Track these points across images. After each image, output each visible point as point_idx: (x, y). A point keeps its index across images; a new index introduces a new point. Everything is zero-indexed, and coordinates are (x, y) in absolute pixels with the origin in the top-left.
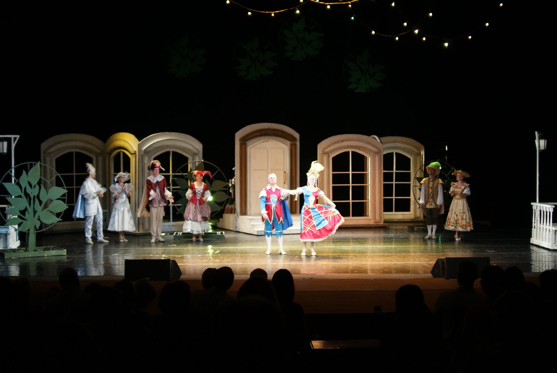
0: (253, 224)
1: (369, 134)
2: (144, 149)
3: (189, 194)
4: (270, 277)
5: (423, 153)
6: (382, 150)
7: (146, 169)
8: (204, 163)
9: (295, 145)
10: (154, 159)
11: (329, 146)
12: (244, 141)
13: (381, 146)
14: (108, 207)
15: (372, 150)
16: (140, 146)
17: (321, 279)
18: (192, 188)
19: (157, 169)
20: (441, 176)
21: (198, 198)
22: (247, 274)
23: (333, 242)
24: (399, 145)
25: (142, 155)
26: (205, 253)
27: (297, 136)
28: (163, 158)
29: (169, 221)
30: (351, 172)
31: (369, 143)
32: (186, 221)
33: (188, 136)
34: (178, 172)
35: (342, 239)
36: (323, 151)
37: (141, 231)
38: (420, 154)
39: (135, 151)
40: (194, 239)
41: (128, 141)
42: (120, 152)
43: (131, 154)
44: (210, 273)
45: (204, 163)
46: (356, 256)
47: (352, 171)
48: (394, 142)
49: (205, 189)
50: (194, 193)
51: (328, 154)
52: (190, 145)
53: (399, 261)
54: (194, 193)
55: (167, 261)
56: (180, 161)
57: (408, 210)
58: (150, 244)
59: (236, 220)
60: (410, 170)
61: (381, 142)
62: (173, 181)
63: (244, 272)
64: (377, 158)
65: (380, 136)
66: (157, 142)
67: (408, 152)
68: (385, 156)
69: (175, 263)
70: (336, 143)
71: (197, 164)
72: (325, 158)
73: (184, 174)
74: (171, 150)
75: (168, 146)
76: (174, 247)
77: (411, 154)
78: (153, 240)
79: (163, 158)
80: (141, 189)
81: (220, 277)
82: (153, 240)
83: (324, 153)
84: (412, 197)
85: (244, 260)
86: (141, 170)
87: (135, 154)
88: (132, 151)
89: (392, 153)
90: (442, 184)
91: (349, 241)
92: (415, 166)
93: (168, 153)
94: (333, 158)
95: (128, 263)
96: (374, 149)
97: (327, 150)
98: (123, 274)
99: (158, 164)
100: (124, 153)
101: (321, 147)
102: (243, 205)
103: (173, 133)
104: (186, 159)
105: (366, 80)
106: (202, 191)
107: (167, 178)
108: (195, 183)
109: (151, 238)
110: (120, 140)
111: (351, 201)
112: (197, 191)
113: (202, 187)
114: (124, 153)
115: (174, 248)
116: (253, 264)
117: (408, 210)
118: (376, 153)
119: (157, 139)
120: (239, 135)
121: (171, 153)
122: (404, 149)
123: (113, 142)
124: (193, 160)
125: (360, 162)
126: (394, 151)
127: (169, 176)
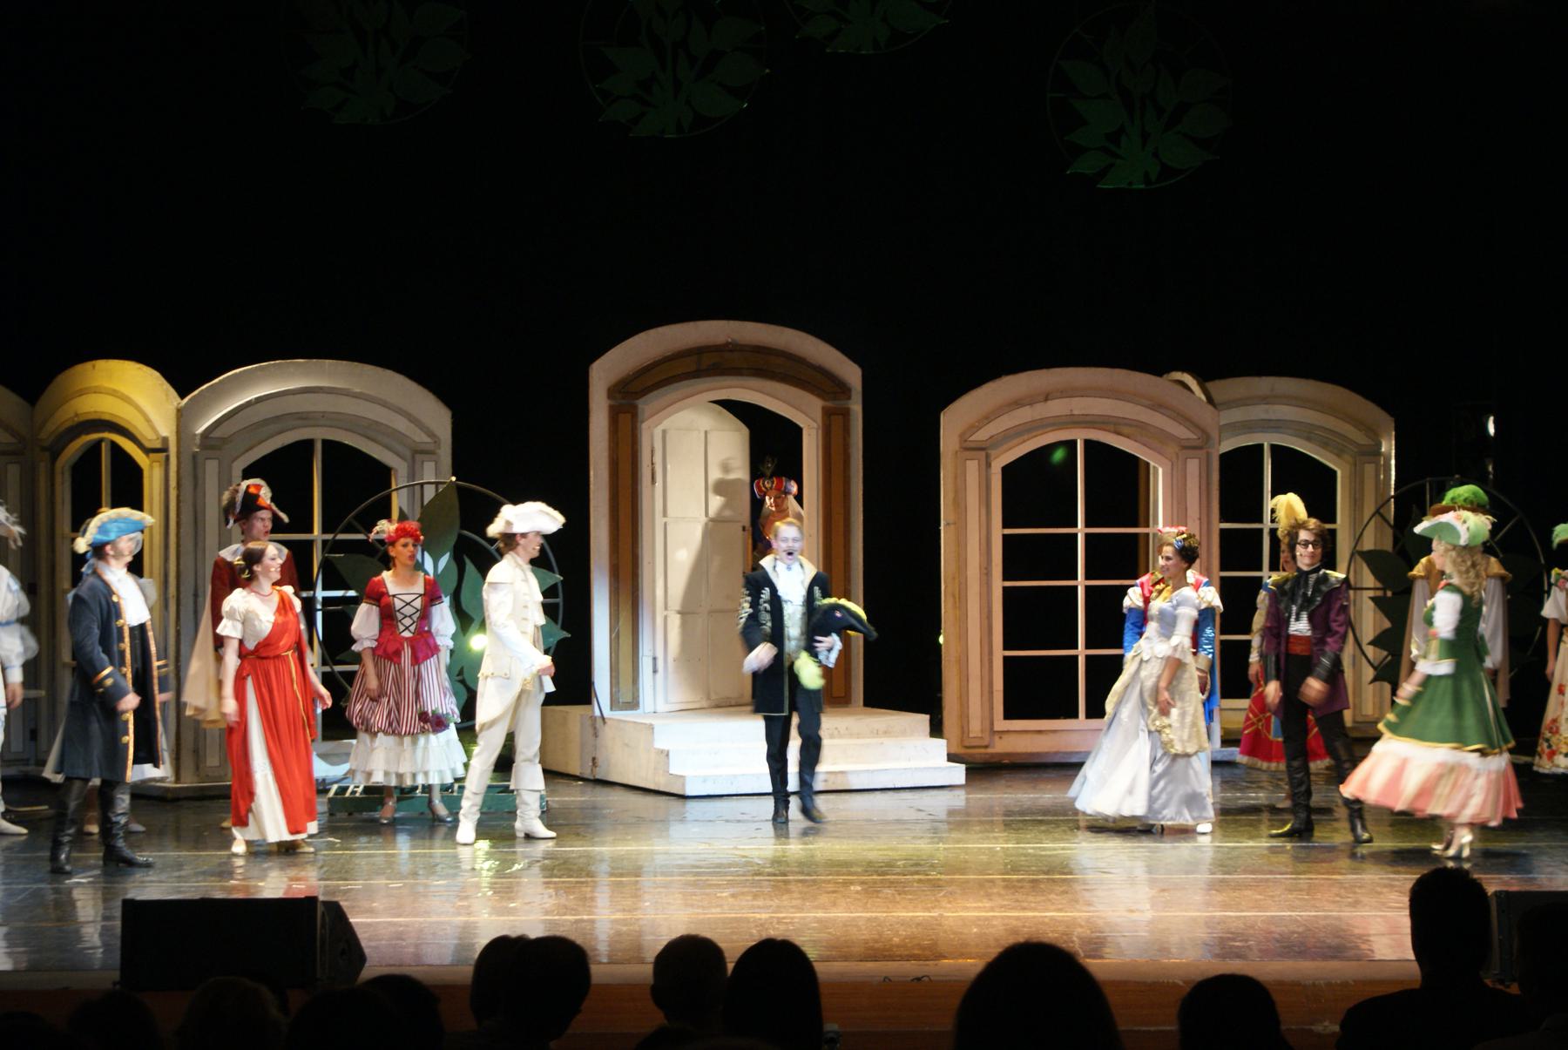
1: (1159, 371)
2: (200, 430)
4: (368, 972)
5: (1388, 446)
6: (1215, 434)
7: (212, 514)
8: (460, 489)
9: (846, 414)
10: (247, 474)
11: (988, 419)
12: (630, 395)
13: (1207, 415)
14: (44, 680)
15: (1167, 429)
17: (1137, 983)
19: (265, 514)
21: (407, 634)
22: (642, 961)
23: (1007, 825)
24: (1279, 412)
25: (194, 456)
27: (852, 373)
28: (284, 469)
30: (1081, 530)
31: (1158, 406)
32: (363, 736)
33: (389, 373)
35: (1046, 812)
36: (963, 438)
37: (189, 782)
38: (1378, 453)
39: (165, 440)
41: (131, 395)
42: (100, 441)
44: (505, 950)
45: (460, 489)
47: (1088, 525)
48: (1266, 400)
50: (388, 616)
51: (983, 450)
52: (399, 418)
53: (1292, 908)
54: (388, 616)
56: (358, 483)
59: (596, 735)
61: (1210, 400)
62: (326, 565)
63: (628, 950)
64: (1193, 466)
65: (1204, 377)
66: (259, 400)
67: (1325, 444)
68: (1226, 459)
69: (335, 912)
70: (1017, 404)
71: (430, 492)
72: (972, 467)
74: (318, 434)
75: (304, 418)
77: (1339, 453)
79: (284, 469)
80: (188, 601)
81: (533, 976)
83: (969, 449)
85: (629, 902)
86: (187, 518)
88: (150, 439)
90: (1502, 578)
92: (1356, 502)
96: (1182, 432)
97: (981, 435)
98: (1415, 969)
100: (116, 449)
102: (625, 666)
105: (1145, 137)
106: (418, 604)
110: (97, 391)
111: (1081, 652)
112: (398, 604)
114: (115, 447)
116: (667, 917)
118: (1187, 447)
119: (254, 389)
120: (604, 373)
121: (318, 447)
122: (1308, 432)
123: (67, 400)
124: (412, 474)
125: (1119, 485)
126: (1267, 440)
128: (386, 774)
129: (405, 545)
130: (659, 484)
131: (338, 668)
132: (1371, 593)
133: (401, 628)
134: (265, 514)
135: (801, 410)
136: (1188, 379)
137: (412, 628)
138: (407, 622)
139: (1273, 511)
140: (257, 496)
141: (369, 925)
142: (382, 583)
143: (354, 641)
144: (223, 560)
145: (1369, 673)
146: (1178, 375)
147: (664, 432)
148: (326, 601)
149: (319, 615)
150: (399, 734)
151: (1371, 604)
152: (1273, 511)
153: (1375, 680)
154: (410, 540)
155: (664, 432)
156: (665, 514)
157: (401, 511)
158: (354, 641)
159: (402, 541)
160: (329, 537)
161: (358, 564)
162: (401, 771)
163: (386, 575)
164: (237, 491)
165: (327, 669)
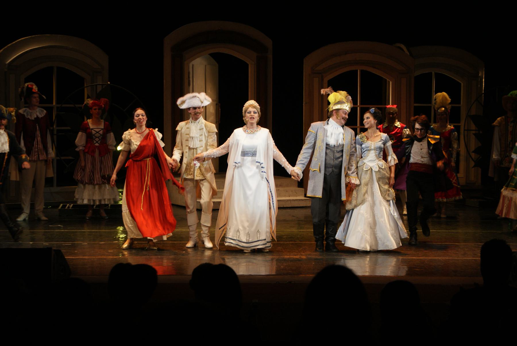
3: (80, 139)
5: (482, 74)
10: (27, 80)
18: (86, 129)
21: (97, 144)
27: (268, 43)
29: (52, 186)
40: (89, 214)
49: (107, 131)
50: (90, 137)
52: (86, 56)
54: (90, 137)
55: (48, 250)
60: (460, 103)
69: (59, 253)
71: (99, 89)
73: (77, 106)
76: (59, 228)
79: (42, 78)
95: (121, 205)
106: (101, 132)
107: (49, 110)
112: (93, 132)
115: (59, 229)
120: (169, 41)
127: (52, 108)
128: (89, 200)
129: (95, 109)
130: (191, 86)
131: (63, 158)
132: (474, 132)
133: (95, 142)
134: (36, 95)
135: (249, 58)
136: (402, 46)
137: (99, 142)
139: (435, 100)
140: (32, 88)
141: (73, 259)
142: (88, 124)
143: (76, 147)
144: (20, 113)
145: (472, 164)
146: (398, 45)
147: (193, 65)
148: (58, 130)
149: (55, 137)
150: (94, 184)
151: (474, 137)
152: (435, 100)
153: (474, 167)
154: (97, 107)
155: (193, 65)
157: (88, 95)
158: (76, 147)
159: (94, 108)
160: (59, 106)
161: (75, 119)
162: (94, 199)
163: (89, 121)
164: (23, 87)
165: (58, 158)
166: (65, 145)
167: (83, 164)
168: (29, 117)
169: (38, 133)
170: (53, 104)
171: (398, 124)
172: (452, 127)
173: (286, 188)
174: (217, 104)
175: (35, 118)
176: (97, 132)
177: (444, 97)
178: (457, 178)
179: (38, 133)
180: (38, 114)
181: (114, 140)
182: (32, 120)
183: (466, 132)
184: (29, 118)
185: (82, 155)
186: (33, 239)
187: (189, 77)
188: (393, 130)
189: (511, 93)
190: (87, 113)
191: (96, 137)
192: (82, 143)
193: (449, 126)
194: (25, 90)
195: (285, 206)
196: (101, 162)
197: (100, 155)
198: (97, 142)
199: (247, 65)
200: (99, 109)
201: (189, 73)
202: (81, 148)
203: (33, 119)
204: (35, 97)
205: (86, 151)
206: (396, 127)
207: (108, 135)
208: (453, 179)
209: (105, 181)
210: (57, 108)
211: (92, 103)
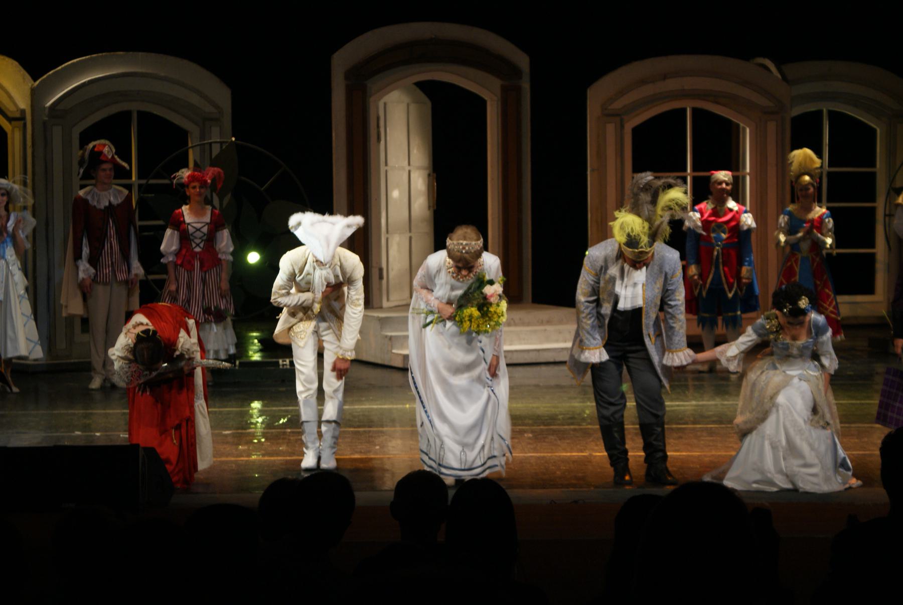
0: (390, 334)
1: (746, 56)
3: (169, 242)
11: (622, 93)
16: (36, 96)
18: (178, 224)
20: (451, 318)
21: (198, 250)
25: (45, 123)
26: (243, 422)
27: (523, 61)
28: (113, 128)
34: (156, 177)
39: (23, 112)
43: (10, 120)
46: (711, 433)
49: (215, 226)
50: (185, 238)
51: (618, 116)
52: (189, 90)
54: (185, 238)
56: (162, 143)
57: (869, 289)
58: (85, 397)
64: (772, 127)
68: (794, 120)
70: (643, 82)
71: (216, 150)
72: (611, 128)
74: (134, 107)
78: (96, 383)
82: (96, 383)
83: (608, 115)
84: (880, 205)
87: (22, 118)
89: (819, 113)
91: (687, 387)
93: (124, 117)
94: (636, 131)
97: (618, 105)
99: (108, 150)
101: (598, 96)
103: (140, 54)
104: (182, 136)
106: (205, 230)
108: (185, 209)
109: (90, 379)
113: (207, 219)
117: (869, 289)
120: (342, 61)
124: (202, 137)
126: (825, 107)
129: (194, 187)
130: (382, 142)
133: (194, 245)
135: (486, 89)
136: (768, 63)
137: (202, 245)
138: (198, 241)
147: (385, 104)
154: (196, 184)
155: (385, 104)
156: (386, 164)
158: (162, 256)
160: (143, 182)
166: (150, 255)
167: (173, 287)
168: (95, 203)
169: (112, 231)
170: (131, 178)
171: (732, 204)
172: (824, 210)
173: (561, 327)
174: (429, 175)
175: (106, 207)
176: (198, 230)
177: (806, 155)
178: (837, 303)
179: (112, 231)
180: (112, 199)
181: (230, 242)
182: (101, 210)
183: (887, 219)
184: (95, 207)
185: (171, 269)
186: (86, 428)
187: (378, 126)
188: (725, 215)
189: (91, 145)
190: (180, 196)
191: (196, 238)
192: (174, 248)
193: (818, 208)
194: (87, 154)
195: (558, 359)
196: (204, 281)
197: (202, 267)
198: (198, 245)
199: (484, 102)
200: (201, 187)
201: (378, 119)
202: (171, 259)
203: (102, 207)
204: (104, 170)
205: (179, 262)
206: (731, 210)
207: (219, 234)
208: (830, 305)
209: (211, 318)
210: (140, 186)
211: (189, 177)
